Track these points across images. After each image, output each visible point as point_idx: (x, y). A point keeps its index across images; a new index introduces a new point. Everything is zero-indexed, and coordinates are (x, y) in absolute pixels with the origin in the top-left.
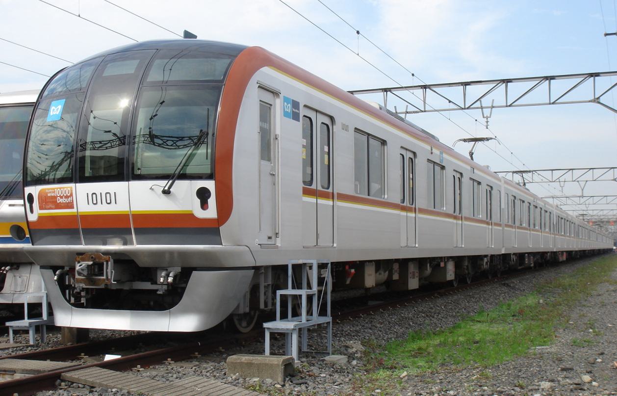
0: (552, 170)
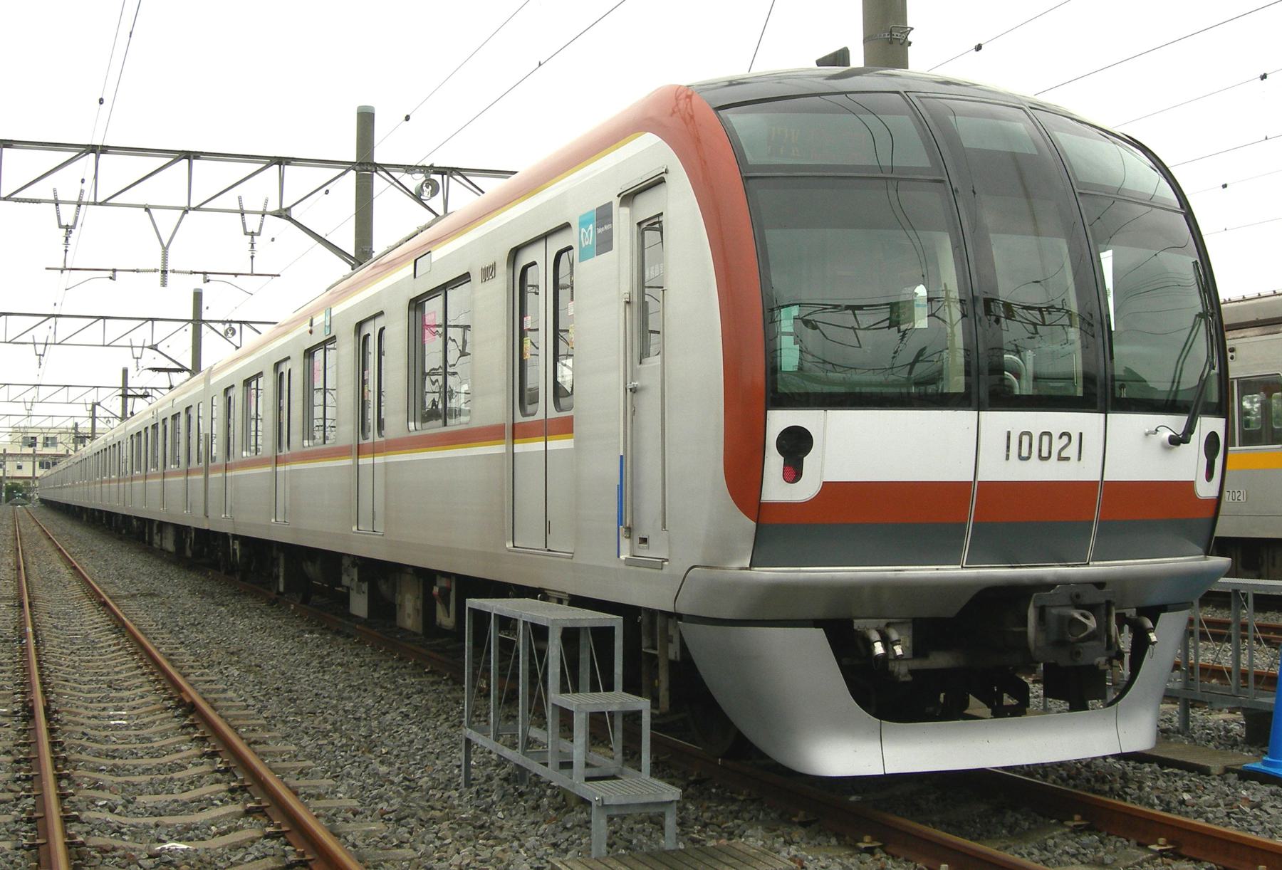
0: (252, 274)
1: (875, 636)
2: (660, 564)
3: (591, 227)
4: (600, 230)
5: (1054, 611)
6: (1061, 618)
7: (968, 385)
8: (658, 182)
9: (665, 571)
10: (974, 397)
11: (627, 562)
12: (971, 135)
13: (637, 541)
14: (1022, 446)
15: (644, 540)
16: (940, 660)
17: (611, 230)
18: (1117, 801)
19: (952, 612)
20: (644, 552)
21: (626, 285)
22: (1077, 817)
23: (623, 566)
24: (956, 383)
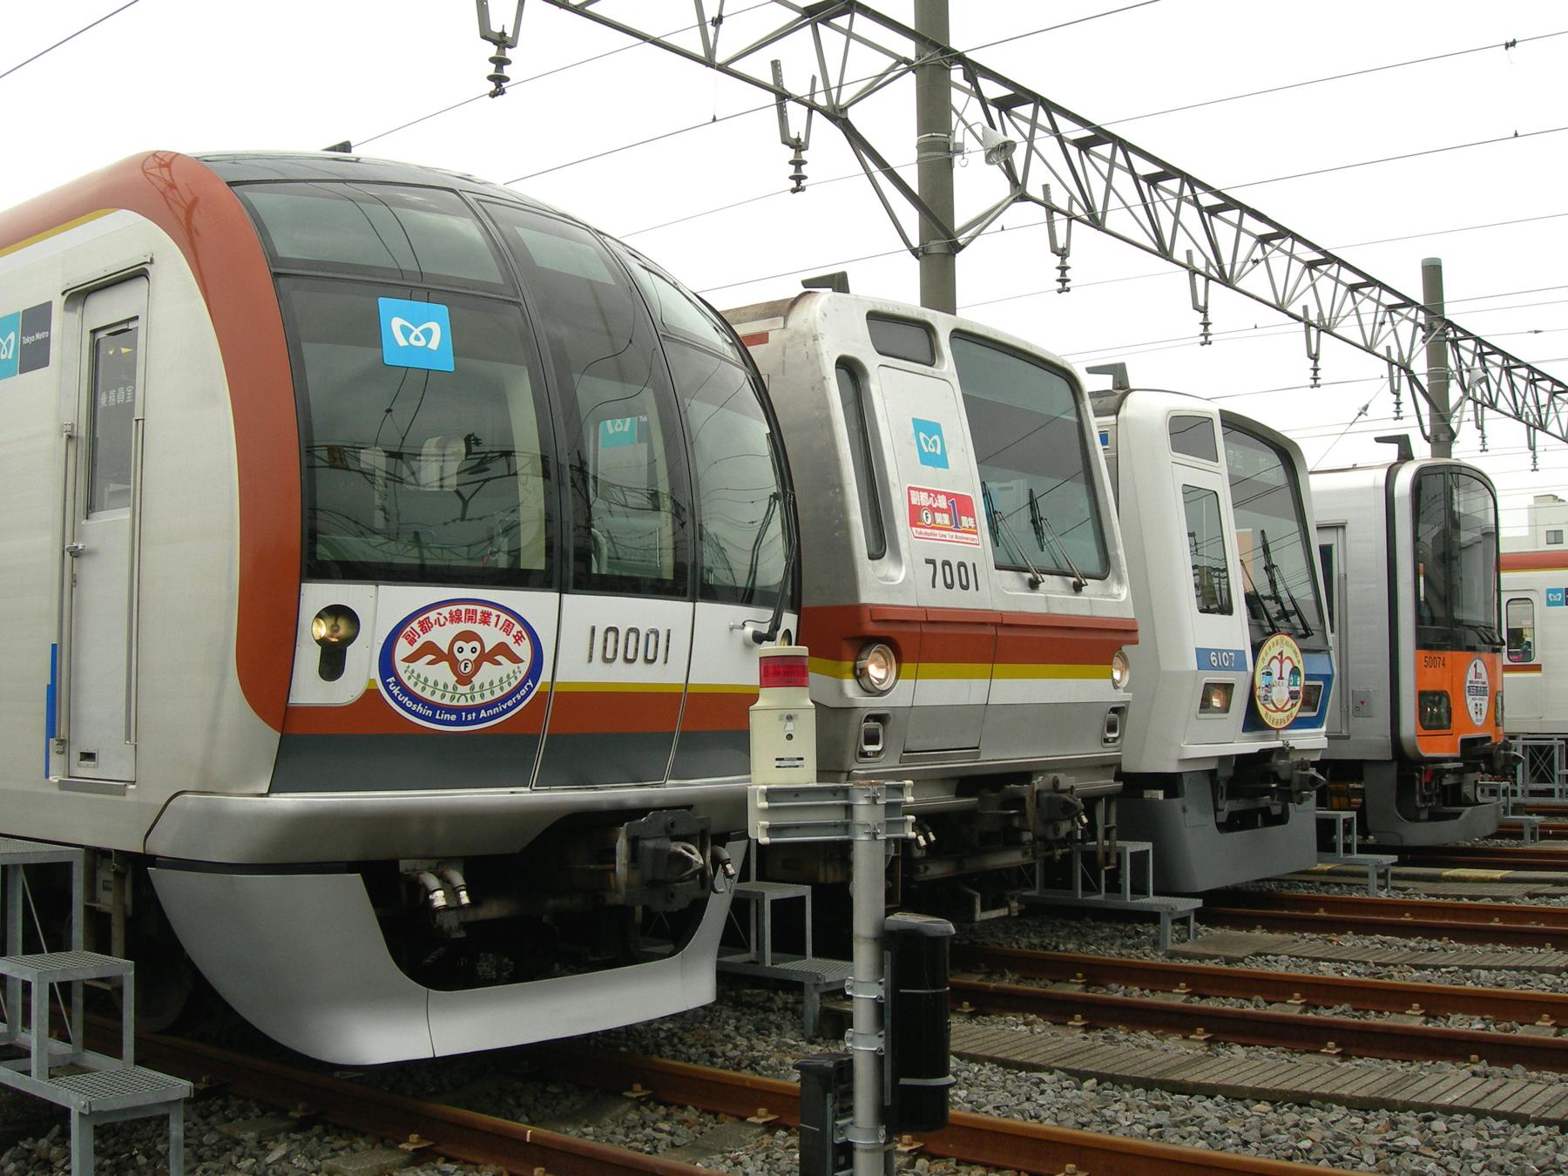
1: (432, 881)
2: (116, 788)
3: (12, 336)
4: (28, 340)
5: (650, 844)
6: (657, 852)
7: (549, 566)
8: (139, 274)
9: (129, 797)
10: (556, 575)
11: (63, 785)
12: (544, 250)
13: (75, 756)
14: (611, 644)
15: (88, 756)
16: (493, 910)
17: (47, 341)
18: (730, 1073)
19: (517, 849)
20: (85, 771)
21: (74, 410)
22: (637, 1087)
23: (56, 791)
24: (534, 560)
